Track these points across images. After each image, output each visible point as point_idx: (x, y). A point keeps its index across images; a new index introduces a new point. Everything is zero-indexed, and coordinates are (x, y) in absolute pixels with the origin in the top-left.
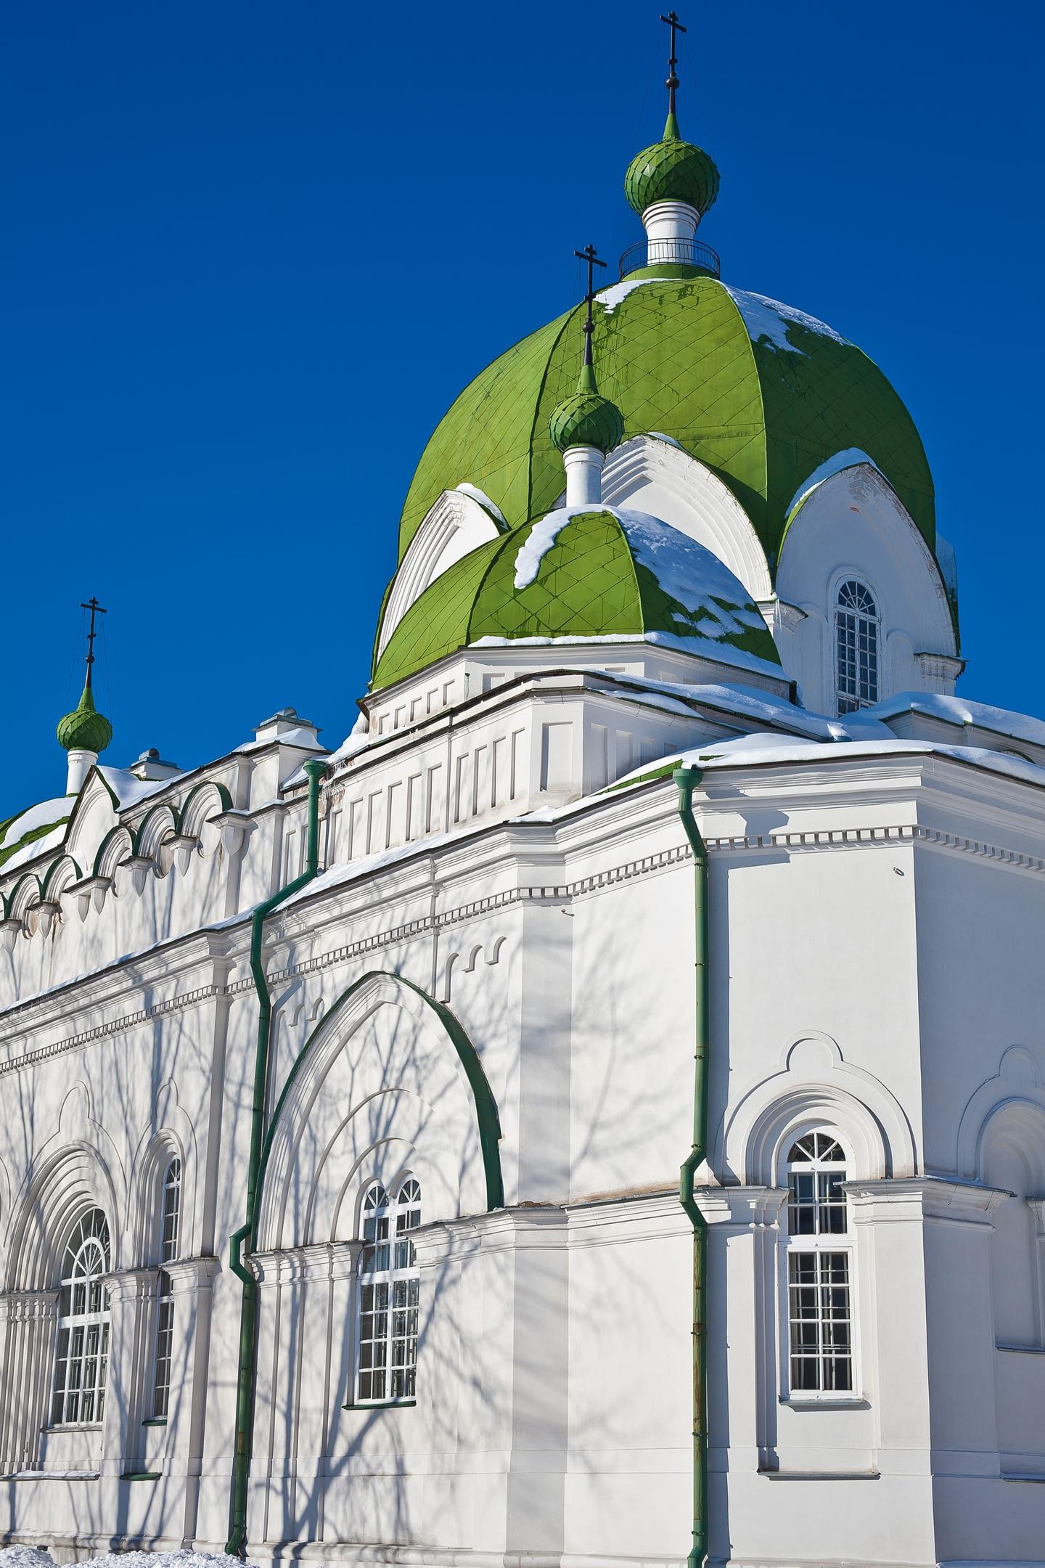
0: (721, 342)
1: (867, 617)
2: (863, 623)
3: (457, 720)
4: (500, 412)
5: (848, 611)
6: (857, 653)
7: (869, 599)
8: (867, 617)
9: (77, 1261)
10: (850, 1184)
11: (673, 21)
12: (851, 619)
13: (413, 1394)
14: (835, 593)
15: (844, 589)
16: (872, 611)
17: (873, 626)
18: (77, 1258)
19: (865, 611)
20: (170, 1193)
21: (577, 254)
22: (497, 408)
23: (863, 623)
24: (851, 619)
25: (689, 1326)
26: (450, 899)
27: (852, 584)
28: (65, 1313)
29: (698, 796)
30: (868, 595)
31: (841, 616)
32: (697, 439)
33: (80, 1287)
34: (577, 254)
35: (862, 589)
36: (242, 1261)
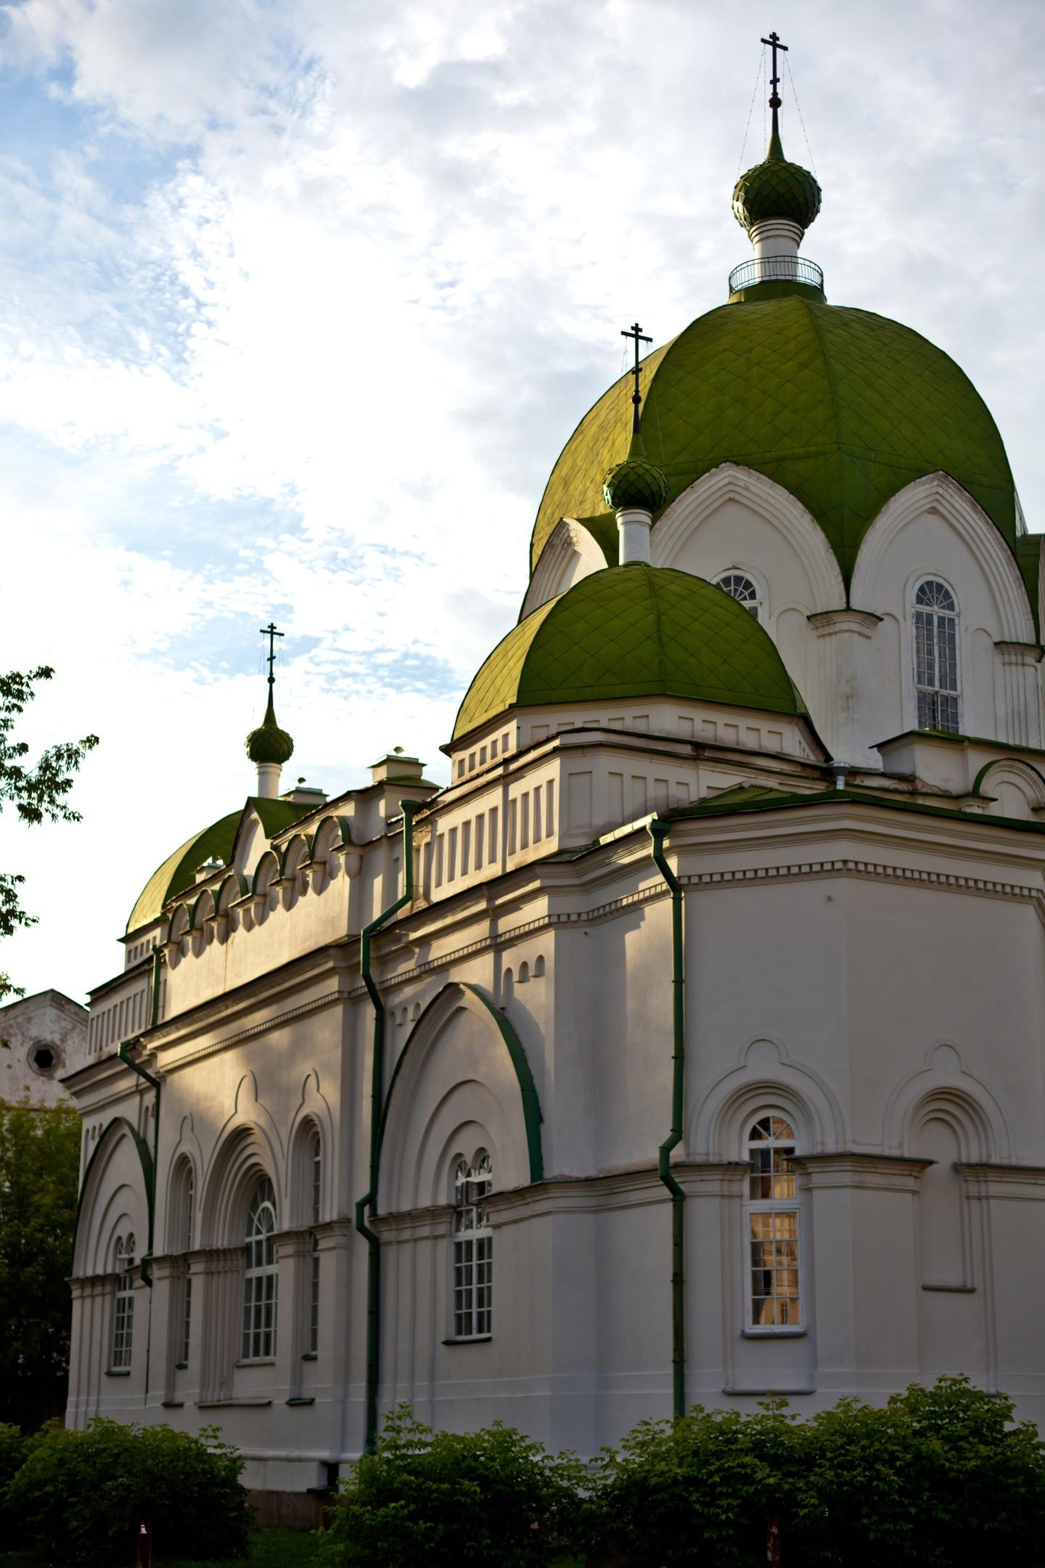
0: (804, 366)
1: (947, 613)
2: (941, 619)
3: (513, 767)
4: (609, 443)
5: (925, 609)
6: (936, 648)
7: (947, 595)
8: (947, 613)
9: (256, 1222)
10: (78, 1279)
11: (774, 41)
12: (930, 616)
13: (489, 1331)
14: (912, 594)
15: (922, 589)
16: (951, 607)
17: (952, 621)
18: (255, 1219)
19: (943, 608)
20: (317, 1164)
21: (623, 333)
22: (607, 440)
23: (941, 619)
24: (930, 616)
25: (670, 1277)
26: (508, 923)
27: (929, 584)
28: (249, 1266)
29: (666, 843)
30: (947, 591)
31: (919, 616)
32: (781, 460)
33: (259, 1243)
34: (623, 333)
35: (940, 586)
36: (366, 1223)
